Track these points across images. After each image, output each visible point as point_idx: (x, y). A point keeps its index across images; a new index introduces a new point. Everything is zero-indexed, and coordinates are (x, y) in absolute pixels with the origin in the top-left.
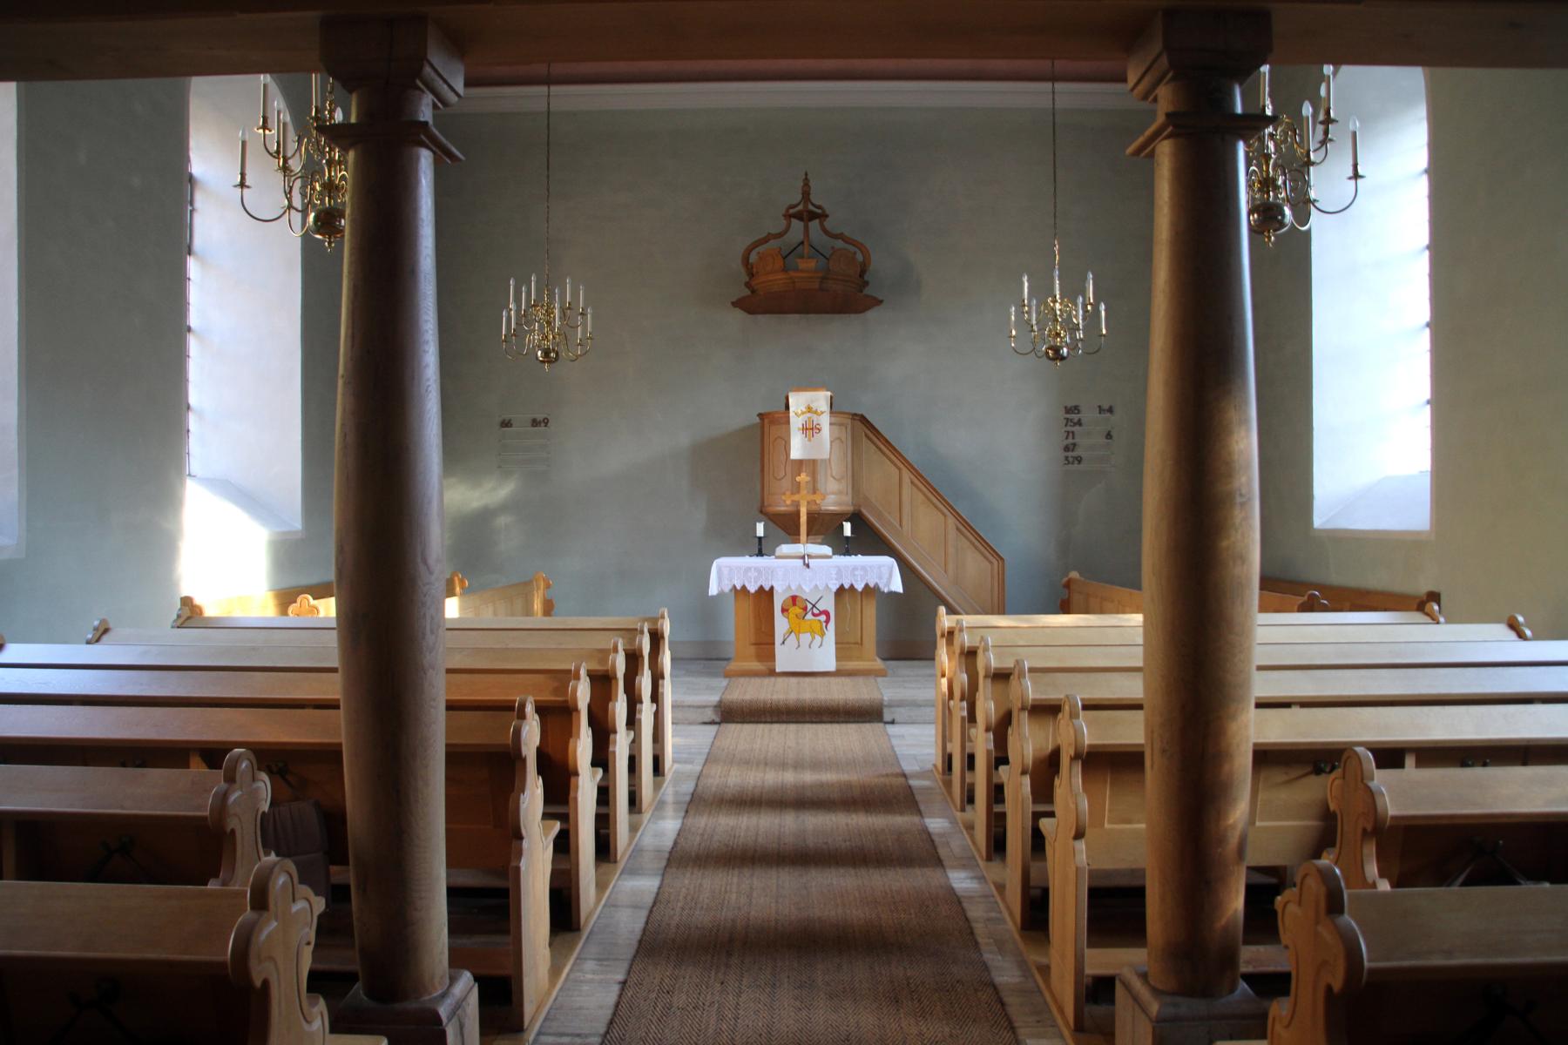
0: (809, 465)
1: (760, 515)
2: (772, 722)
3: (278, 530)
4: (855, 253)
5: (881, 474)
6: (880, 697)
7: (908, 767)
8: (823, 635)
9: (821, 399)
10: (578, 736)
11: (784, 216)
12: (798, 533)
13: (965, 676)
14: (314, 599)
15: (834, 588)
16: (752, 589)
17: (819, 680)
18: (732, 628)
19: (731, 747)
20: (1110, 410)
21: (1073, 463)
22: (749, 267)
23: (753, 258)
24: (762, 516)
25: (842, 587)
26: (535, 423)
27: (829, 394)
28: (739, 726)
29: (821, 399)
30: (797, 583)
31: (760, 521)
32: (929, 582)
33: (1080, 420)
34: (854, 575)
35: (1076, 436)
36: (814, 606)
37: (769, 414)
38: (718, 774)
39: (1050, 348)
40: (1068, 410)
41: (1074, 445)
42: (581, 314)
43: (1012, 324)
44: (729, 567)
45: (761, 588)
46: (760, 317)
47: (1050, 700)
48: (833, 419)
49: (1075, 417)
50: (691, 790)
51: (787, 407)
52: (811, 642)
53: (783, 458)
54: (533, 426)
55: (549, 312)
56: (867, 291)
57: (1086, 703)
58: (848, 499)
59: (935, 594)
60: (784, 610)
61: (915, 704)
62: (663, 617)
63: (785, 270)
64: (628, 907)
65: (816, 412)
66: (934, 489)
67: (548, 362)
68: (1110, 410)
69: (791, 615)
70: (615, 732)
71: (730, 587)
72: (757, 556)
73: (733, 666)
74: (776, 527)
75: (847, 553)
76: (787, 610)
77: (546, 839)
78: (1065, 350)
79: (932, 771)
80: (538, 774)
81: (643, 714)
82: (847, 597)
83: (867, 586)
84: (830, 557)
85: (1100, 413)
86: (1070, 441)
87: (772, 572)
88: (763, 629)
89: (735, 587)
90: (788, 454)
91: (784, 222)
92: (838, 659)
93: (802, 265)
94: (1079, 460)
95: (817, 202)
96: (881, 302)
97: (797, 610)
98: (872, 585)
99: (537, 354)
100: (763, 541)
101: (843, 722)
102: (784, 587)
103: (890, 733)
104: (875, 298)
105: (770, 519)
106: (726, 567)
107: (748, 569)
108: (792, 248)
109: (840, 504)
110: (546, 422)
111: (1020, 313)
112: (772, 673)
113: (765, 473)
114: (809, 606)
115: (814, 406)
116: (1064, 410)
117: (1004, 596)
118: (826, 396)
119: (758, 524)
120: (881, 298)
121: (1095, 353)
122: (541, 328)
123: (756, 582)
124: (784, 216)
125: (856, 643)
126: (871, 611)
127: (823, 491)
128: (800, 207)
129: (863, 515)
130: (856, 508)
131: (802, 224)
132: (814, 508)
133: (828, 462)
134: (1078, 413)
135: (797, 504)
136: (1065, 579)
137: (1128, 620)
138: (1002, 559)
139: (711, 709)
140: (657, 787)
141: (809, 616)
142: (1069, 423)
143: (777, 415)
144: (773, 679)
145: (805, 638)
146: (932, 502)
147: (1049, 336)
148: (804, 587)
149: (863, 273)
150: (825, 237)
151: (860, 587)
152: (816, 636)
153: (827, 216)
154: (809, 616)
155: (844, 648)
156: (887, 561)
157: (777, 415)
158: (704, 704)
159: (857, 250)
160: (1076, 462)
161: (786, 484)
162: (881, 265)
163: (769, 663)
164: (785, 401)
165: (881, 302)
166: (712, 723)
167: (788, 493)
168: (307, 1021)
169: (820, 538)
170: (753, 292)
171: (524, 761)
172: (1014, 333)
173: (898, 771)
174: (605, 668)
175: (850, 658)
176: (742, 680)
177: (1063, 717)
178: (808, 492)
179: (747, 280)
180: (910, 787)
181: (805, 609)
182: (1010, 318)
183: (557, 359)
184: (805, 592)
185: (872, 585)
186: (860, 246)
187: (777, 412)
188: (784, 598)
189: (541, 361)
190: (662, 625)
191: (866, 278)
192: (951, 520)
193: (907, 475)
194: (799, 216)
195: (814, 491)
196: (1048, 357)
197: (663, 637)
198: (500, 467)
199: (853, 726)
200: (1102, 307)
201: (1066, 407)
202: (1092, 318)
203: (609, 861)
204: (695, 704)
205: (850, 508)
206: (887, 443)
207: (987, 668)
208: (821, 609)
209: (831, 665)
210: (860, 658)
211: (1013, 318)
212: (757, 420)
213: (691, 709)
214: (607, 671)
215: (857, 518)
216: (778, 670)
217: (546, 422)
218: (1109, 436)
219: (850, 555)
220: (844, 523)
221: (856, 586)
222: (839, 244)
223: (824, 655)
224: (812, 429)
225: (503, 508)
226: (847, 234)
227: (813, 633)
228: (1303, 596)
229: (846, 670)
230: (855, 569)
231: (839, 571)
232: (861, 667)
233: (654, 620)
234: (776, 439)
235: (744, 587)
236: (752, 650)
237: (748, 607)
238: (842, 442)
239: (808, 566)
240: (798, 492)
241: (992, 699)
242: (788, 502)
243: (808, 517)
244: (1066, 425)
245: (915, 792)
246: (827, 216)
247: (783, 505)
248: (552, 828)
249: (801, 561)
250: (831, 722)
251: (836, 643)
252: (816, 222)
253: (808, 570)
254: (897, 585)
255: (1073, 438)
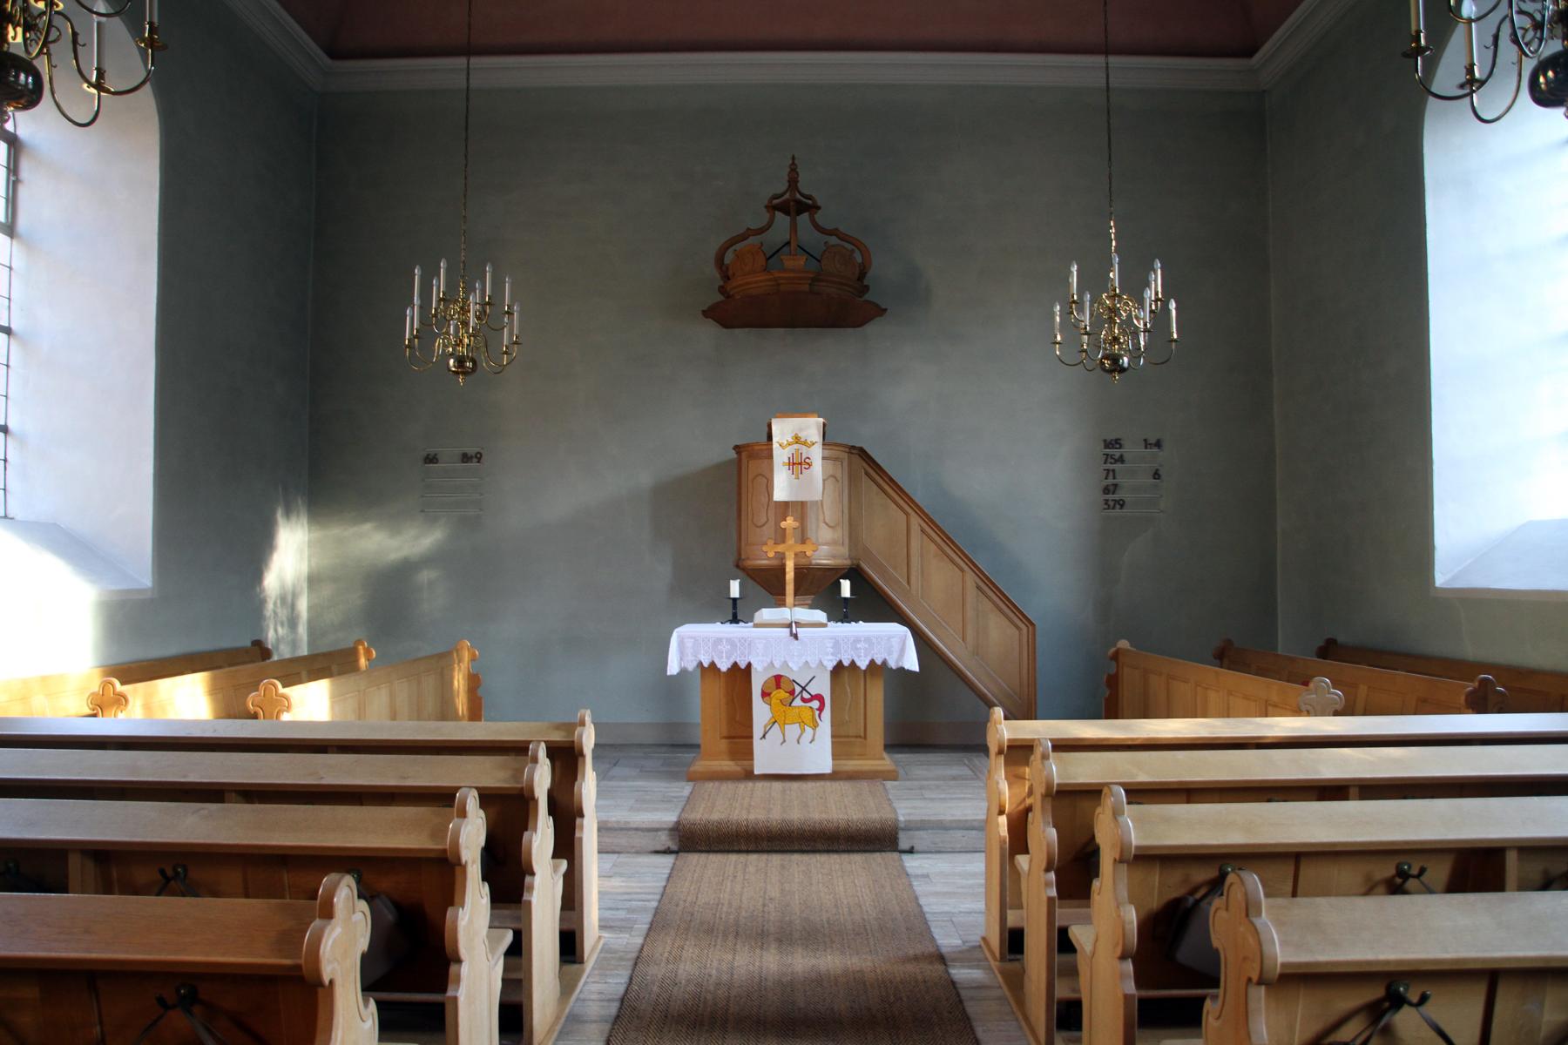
0: (797, 508)
1: (735, 569)
2: (748, 852)
3: (113, 587)
4: (853, 251)
5: (885, 520)
6: (893, 816)
7: (947, 940)
8: (815, 726)
9: (811, 427)
10: (535, 829)
11: (766, 207)
12: (782, 592)
13: (1053, 833)
14: (123, 683)
15: (830, 665)
16: (724, 666)
17: (810, 785)
18: (701, 712)
19: (689, 899)
20: (1158, 444)
21: (1113, 508)
22: (724, 268)
23: (729, 257)
24: (740, 572)
25: (839, 665)
26: (466, 458)
27: (821, 420)
28: (703, 857)
29: (811, 427)
30: (783, 659)
31: (734, 579)
32: (951, 661)
33: (1121, 456)
34: (857, 649)
35: (1117, 476)
36: (804, 689)
37: (748, 445)
38: (666, 955)
39: (1106, 357)
40: (1108, 444)
41: (1116, 486)
42: (508, 313)
43: (1057, 326)
44: (694, 638)
45: (735, 664)
46: (737, 331)
47: (1318, 964)
48: (826, 452)
49: (1116, 452)
50: (622, 989)
51: (770, 437)
52: (800, 737)
53: (764, 500)
54: (463, 462)
55: (464, 310)
56: (867, 297)
57: (1055, 743)
58: (844, 550)
59: (941, 657)
60: (765, 694)
61: (942, 826)
62: (582, 724)
63: (766, 269)
64: (595, 1022)
65: (805, 443)
66: (949, 538)
67: (464, 373)
68: (1158, 444)
69: (774, 701)
70: (582, 816)
71: (695, 664)
72: (731, 623)
73: (701, 766)
74: (755, 583)
75: (845, 619)
76: (769, 694)
77: (493, 958)
78: (1126, 359)
79: (980, 946)
80: (549, 814)
81: (535, 893)
82: (846, 677)
83: (872, 662)
84: (824, 625)
85: (1146, 448)
86: (1110, 481)
87: (749, 645)
88: (737, 719)
89: (700, 664)
90: (770, 493)
91: (767, 216)
92: (835, 756)
93: (789, 263)
94: (1121, 504)
95: (806, 192)
96: (885, 310)
97: (782, 694)
98: (879, 662)
99: (448, 364)
100: (738, 602)
101: (844, 851)
102: (766, 665)
103: (910, 871)
104: (877, 306)
105: (748, 575)
106: (691, 638)
107: (718, 641)
108: (775, 250)
109: (834, 557)
110: (479, 457)
111: (1067, 313)
112: (749, 775)
113: (743, 518)
114: (798, 689)
115: (803, 435)
116: (1102, 445)
117: (1035, 669)
118: (817, 423)
119: (731, 581)
120: (883, 307)
121: (1163, 363)
122: (457, 328)
123: (728, 658)
124: (766, 207)
125: (858, 737)
126: (877, 695)
127: (814, 540)
128: (787, 196)
129: (862, 569)
130: (855, 562)
131: (788, 218)
132: (803, 561)
133: (820, 503)
134: (1120, 448)
135: (781, 557)
136: (1113, 650)
137: (1270, 726)
138: (1032, 624)
139: (666, 832)
140: (567, 986)
141: (798, 702)
142: (1109, 460)
143: (757, 448)
144: (750, 784)
145: (793, 730)
146: (948, 556)
147: (1105, 341)
148: (790, 664)
149: (862, 275)
150: (818, 235)
151: (863, 664)
152: (807, 728)
153: (819, 208)
154: (798, 702)
155: (839, 742)
156: (895, 631)
157: (757, 448)
158: (657, 826)
159: (854, 247)
160: (1118, 506)
161: (768, 530)
162: (884, 270)
163: (745, 763)
164: (766, 429)
165: (885, 310)
166: (667, 852)
167: (771, 542)
168: (363, 1021)
169: (809, 599)
170: (728, 297)
171: (536, 802)
172: (1059, 338)
173: (932, 950)
174: (519, 786)
175: (849, 756)
176: (710, 785)
177: (1036, 758)
178: (796, 542)
179: (722, 283)
180: (953, 983)
181: (792, 692)
182: (1054, 318)
183: (474, 369)
184: (792, 670)
185: (879, 662)
186: (857, 244)
187: (757, 444)
188: (765, 678)
189: (453, 371)
190: (581, 736)
191: (866, 283)
192: (970, 578)
193: (916, 521)
194: (784, 208)
195: (803, 541)
196: (1104, 369)
197: (582, 754)
198: (422, 511)
199: (857, 858)
200: (1173, 305)
201: (1105, 441)
202: (1160, 316)
203: (574, 962)
204: (644, 826)
205: (844, 561)
206: (892, 482)
207: (1124, 847)
208: (813, 694)
209: (826, 766)
210: (862, 756)
211: (1058, 319)
212: (733, 455)
213: (640, 833)
214: (445, 851)
215: (855, 573)
216: (756, 772)
217: (479, 457)
218: (1156, 475)
219: (849, 622)
220: (841, 581)
221: (858, 663)
222: (833, 240)
223: (816, 753)
224: (801, 464)
225: (427, 561)
226: (842, 229)
227: (802, 723)
228: (1472, 681)
229: (847, 772)
230: (857, 640)
231: (837, 643)
232: (866, 768)
233: (571, 727)
234: (757, 476)
235: (713, 664)
236: (723, 745)
237: (718, 689)
238: (837, 480)
239: (796, 637)
240: (784, 541)
241: (1131, 902)
242: (771, 555)
243: (795, 573)
244: (1105, 463)
245: (963, 993)
246: (819, 208)
247: (765, 555)
248: (501, 938)
249: (788, 630)
250: (828, 851)
251: (833, 737)
252: (805, 216)
253: (796, 642)
254: (912, 662)
255: (1114, 478)
